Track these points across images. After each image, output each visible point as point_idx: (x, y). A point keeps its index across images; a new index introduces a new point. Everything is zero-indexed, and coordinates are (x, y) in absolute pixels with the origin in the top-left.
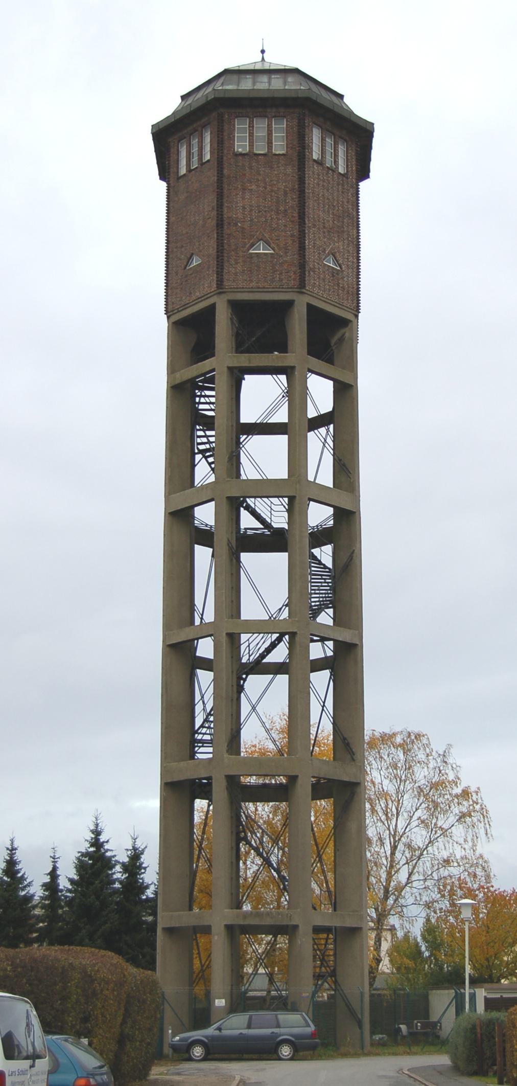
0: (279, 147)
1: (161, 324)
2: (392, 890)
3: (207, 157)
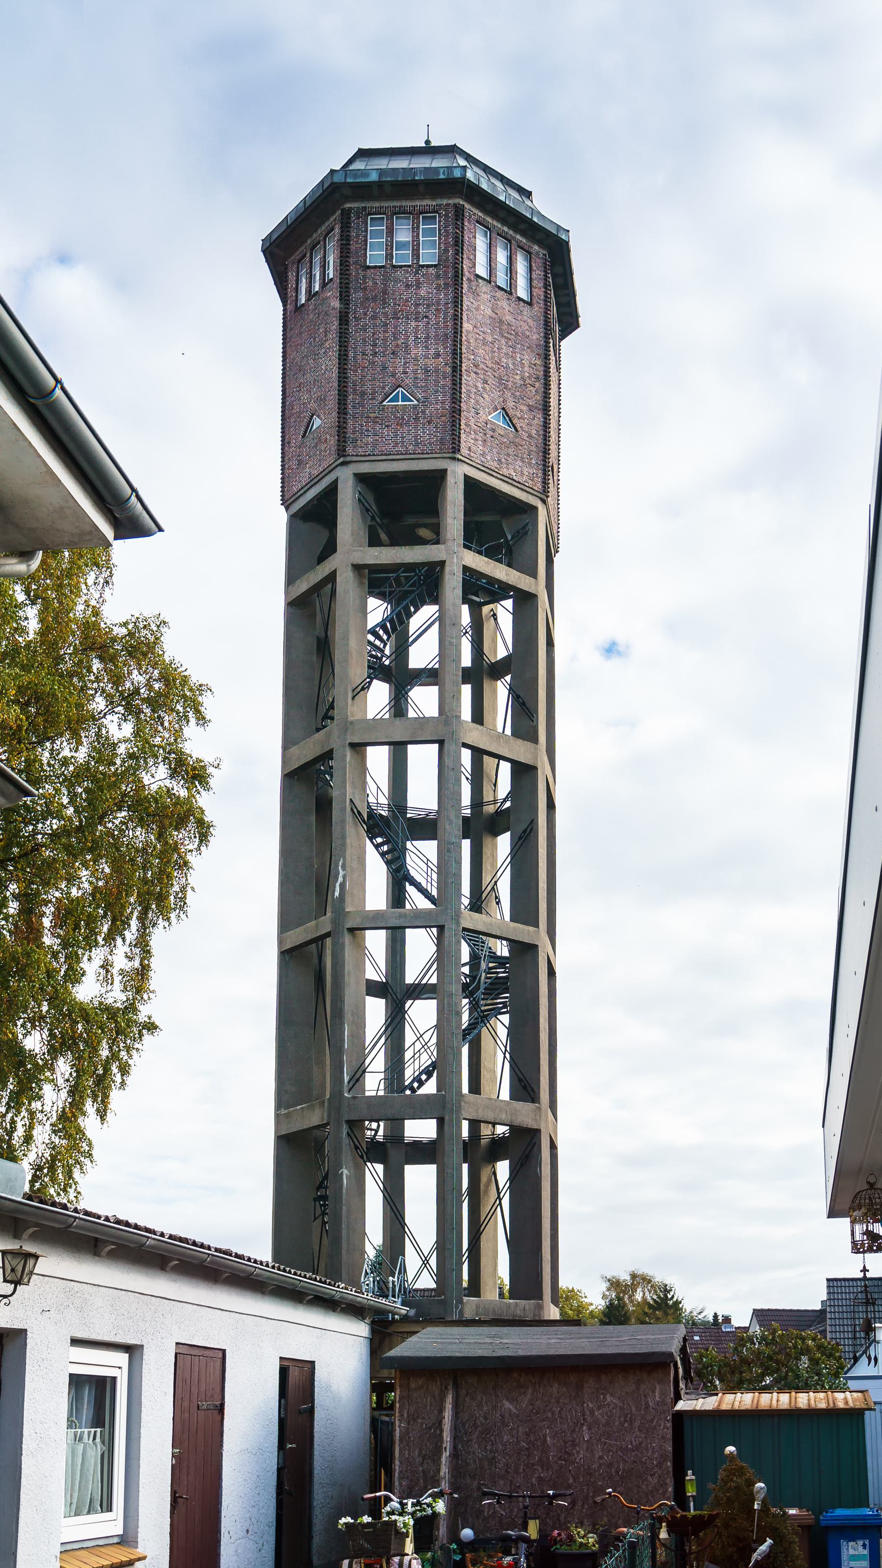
0: (429, 255)
1: (280, 518)
2: (591, 1537)
3: (331, 273)
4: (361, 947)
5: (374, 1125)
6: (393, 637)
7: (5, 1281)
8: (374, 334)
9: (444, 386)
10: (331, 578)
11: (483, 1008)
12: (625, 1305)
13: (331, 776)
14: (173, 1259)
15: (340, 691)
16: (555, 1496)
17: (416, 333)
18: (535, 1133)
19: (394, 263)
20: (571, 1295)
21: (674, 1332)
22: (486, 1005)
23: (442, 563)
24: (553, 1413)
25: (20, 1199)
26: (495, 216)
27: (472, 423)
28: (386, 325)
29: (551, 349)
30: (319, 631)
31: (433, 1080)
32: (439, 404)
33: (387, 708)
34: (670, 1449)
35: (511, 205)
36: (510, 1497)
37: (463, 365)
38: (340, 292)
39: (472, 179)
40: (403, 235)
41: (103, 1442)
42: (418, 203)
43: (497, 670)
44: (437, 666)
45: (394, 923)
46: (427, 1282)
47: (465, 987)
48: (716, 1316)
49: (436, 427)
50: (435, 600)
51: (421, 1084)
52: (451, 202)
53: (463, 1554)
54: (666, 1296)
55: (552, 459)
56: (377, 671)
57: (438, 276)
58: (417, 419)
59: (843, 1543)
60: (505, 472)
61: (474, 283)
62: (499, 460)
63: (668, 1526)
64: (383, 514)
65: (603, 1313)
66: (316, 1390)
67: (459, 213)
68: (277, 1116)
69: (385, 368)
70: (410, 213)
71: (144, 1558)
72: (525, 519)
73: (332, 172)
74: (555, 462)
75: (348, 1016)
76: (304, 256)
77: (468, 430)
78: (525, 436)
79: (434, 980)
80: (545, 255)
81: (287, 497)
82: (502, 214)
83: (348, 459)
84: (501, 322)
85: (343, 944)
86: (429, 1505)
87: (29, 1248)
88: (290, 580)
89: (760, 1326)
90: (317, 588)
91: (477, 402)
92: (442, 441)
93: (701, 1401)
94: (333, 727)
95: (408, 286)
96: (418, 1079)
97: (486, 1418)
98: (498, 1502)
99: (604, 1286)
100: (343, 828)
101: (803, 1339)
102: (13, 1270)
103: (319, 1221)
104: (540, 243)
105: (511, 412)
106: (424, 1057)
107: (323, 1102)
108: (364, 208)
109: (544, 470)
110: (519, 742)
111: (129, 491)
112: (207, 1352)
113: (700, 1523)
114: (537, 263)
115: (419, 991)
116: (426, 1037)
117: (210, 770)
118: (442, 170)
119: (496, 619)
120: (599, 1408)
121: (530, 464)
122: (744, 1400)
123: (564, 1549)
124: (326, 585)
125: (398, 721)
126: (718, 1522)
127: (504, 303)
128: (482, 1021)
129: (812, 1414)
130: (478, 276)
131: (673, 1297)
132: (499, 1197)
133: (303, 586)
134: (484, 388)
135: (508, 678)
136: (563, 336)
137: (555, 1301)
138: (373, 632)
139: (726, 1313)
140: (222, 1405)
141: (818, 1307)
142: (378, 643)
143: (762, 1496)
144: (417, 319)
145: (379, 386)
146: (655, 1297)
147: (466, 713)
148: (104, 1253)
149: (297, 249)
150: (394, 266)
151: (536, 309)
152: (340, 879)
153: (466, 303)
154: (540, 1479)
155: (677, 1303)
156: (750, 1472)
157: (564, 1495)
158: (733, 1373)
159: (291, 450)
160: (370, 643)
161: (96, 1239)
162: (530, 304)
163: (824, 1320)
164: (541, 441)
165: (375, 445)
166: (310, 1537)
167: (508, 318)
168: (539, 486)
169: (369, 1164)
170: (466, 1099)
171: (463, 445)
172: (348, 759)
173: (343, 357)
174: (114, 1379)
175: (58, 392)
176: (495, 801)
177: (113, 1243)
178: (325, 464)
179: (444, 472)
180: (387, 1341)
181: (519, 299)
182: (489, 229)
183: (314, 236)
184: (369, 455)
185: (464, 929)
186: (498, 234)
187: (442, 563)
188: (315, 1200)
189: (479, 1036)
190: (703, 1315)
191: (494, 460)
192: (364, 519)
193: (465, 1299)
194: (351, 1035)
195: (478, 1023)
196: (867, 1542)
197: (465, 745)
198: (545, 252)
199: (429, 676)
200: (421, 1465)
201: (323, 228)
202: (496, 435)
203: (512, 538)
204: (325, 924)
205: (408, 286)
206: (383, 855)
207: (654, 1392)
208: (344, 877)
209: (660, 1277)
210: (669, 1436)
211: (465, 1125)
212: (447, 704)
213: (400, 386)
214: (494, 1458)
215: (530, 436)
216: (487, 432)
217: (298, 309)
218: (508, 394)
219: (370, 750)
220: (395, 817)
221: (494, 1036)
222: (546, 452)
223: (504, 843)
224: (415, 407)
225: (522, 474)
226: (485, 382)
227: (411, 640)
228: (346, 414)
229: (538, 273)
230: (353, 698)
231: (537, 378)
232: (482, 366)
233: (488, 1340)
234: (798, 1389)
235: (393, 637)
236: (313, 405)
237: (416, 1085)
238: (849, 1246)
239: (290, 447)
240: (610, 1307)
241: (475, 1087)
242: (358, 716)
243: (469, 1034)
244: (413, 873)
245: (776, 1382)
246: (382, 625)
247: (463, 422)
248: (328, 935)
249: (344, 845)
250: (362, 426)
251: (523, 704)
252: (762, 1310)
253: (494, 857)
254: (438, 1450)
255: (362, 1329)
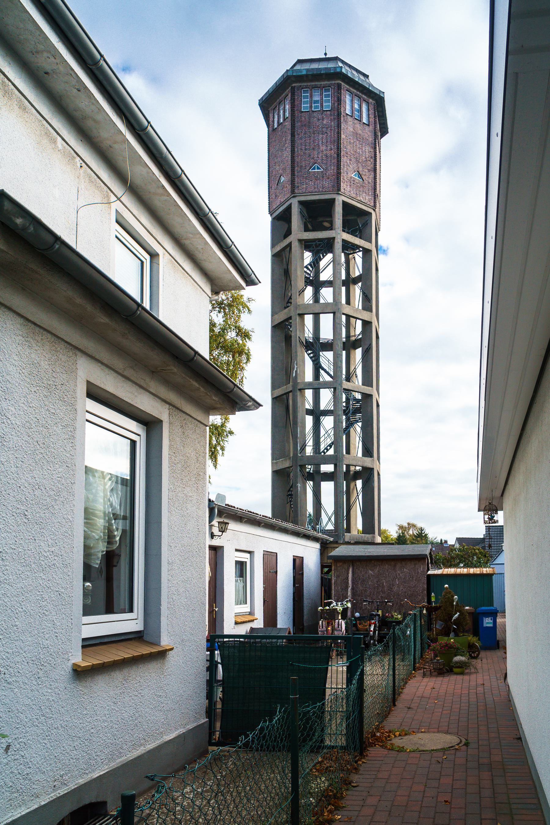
0: (327, 105)
1: (268, 219)
3: (287, 115)
4: (303, 396)
5: (310, 467)
6: (314, 270)
7: (219, 531)
8: (305, 141)
9: (334, 162)
10: (290, 245)
11: (351, 420)
12: (405, 536)
13: (291, 327)
14: (262, 523)
15: (294, 292)
16: (387, 602)
17: (322, 140)
18: (372, 470)
19: (313, 109)
20: (385, 531)
21: (427, 547)
22: (353, 419)
23: (334, 238)
24: (386, 575)
25: (224, 506)
26: (354, 87)
27: (345, 178)
28: (310, 136)
29: (377, 144)
30: (285, 266)
31: (332, 449)
32: (332, 170)
33: (312, 298)
34: (426, 587)
35: (361, 83)
36: (373, 602)
37: (342, 153)
38: (291, 123)
39: (344, 72)
40: (316, 98)
41: (243, 582)
42: (322, 83)
43: (355, 281)
44: (332, 279)
45: (316, 386)
46: (330, 527)
47: (344, 411)
48: (441, 540)
49: (331, 180)
50: (331, 252)
51: (328, 450)
52: (336, 82)
53: (356, 621)
54: (421, 532)
55: (378, 192)
56: (308, 282)
57: (331, 115)
58: (323, 177)
59: (484, 618)
60: (359, 198)
61: (346, 118)
62: (356, 193)
63: (426, 609)
64: (310, 217)
65: (396, 539)
66: (304, 567)
67: (339, 87)
68: (272, 463)
69: (310, 155)
70: (319, 88)
71: (257, 619)
72: (367, 218)
73: (287, 71)
74: (379, 192)
75: (299, 424)
76: (276, 107)
77: (344, 181)
78: (367, 182)
79: (332, 409)
80: (374, 103)
81: (271, 211)
82: (357, 86)
83: (295, 195)
84: (357, 134)
85: (297, 395)
86: (345, 605)
87: (226, 521)
88: (273, 245)
89: (459, 544)
90: (283, 249)
91: (347, 169)
92: (333, 186)
93: (436, 571)
94: (292, 307)
95: (319, 120)
96: (326, 449)
97: (363, 576)
98: (369, 604)
99: (397, 528)
100: (296, 349)
101: (475, 550)
102: (222, 528)
103: (289, 504)
104: (373, 98)
105: (361, 173)
106: (329, 440)
107: (290, 458)
108: (300, 86)
109: (375, 197)
110: (365, 312)
111: (208, 211)
112: (272, 554)
113: (436, 609)
114: (371, 107)
115: (326, 413)
116: (329, 432)
117: (250, 333)
118: (332, 69)
119: (355, 259)
120: (402, 573)
121: (369, 194)
122: (451, 571)
123: (390, 620)
124: (287, 248)
125: (317, 304)
126: (442, 608)
127: (358, 126)
128: (351, 425)
129: (475, 575)
130: (347, 114)
131: (424, 532)
132: (358, 495)
133: (278, 248)
134: (350, 163)
135: (360, 284)
136: (381, 138)
137: (380, 535)
138: (306, 267)
139: (445, 539)
140: (277, 571)
141: (482, 537)
142: (308, 271)
143: (456, 600)
144: (322, 134)
145: (308, 163)
146: (417, 533)
147: (344, 301)
148: (243, 522)
149: (273, 103)
150: (313, 111)
151: (371, 127)
152: (295, 369)
153: (342, 126)
154: (382, 597)
155: (426, 535)
156: (453, 593)
157: (390, 601)
158: (448, 562)
159: (272, 191)
160: (305, 272)
161: (241, 517)
162: (368, 125)
163: (485, 542)
164: (373, 184)
165: (306, 189)
166: (303, 616)
167: (360, 132)
168: (372, 204)
169: (308, 481)
170: (345, 457)
171: (342, 188)
172: (298, 320)
173: (293, 151)
174: (246, 562)
175: (149, 128)
176: (355, 336)
177: (246, 518)
178: (286, 197)
179: (335, 199)
180: (326, 550)
181: (364, 123)
182: (352, 93)
183: (280, 98)
184: (304, 193)
185: (344, 389)
186: (355, 95)
187: (334, 238)
188: (287, 496)
189: (349, 432)
190: (436, 540)
191: (354, 193)
192: (302, 220)
193: (346, 534)
194: (301, 432)
195: (349, 426)
196: (492, 618)
197: (344, 314)
198: (374, 102)
199: (329, 283)
200: (341, 592)
201: (284, 95)
202: (355, 183)
203: (362, 226)
204: (289, 387)
205: (319, 120)
206: (311, 358)
207: (420, 568)
208: (297, 368)
209: (419, 525)
210: (426, 583)
211: (345, 466)
212: (336, 295)
213: (316, 163)
214: (366, 590)
215: (369, 183)
216: (351, 181)
217: (274, 130)
218: (360, 165)
219: (306, 316)
220: (315, 342)
221: (355, 430)
222: (375, 189)
223: (358, 353)
224: (322, 172)
225: (366, 199)
226: (350, 160)
227: (321, 271)
228: (294, 175)
229: (372, 111)
230: (299, 295)
231: (372, 157)
232: (349, 153)
233: (363, 550)
234: (472, 567)
235: (314, 270)
236: (281, 172)
237: (325, 451)
238: (483, 522)
239: (272, 189)
240: (399, 536)
241: (348, 452)
242: (301, 303)
243: (346, 431)
244: (323, 365)
245: (464, 565)
246: (310, 264)
247: (342, 178)
248: (291, 391)
249: (296, 355)
250: (301, 180)
251: (366, 296)
252: (460, 538)
253: (355, 361)
254: (347, 587)
255: (317, 546)
